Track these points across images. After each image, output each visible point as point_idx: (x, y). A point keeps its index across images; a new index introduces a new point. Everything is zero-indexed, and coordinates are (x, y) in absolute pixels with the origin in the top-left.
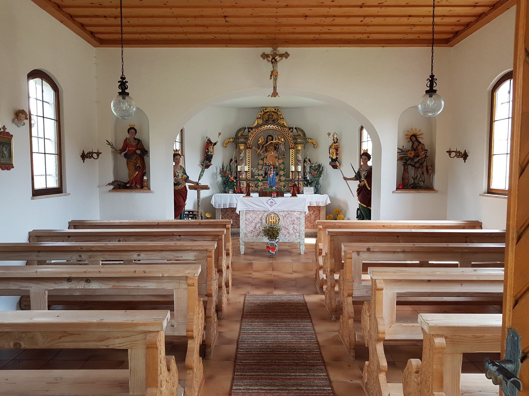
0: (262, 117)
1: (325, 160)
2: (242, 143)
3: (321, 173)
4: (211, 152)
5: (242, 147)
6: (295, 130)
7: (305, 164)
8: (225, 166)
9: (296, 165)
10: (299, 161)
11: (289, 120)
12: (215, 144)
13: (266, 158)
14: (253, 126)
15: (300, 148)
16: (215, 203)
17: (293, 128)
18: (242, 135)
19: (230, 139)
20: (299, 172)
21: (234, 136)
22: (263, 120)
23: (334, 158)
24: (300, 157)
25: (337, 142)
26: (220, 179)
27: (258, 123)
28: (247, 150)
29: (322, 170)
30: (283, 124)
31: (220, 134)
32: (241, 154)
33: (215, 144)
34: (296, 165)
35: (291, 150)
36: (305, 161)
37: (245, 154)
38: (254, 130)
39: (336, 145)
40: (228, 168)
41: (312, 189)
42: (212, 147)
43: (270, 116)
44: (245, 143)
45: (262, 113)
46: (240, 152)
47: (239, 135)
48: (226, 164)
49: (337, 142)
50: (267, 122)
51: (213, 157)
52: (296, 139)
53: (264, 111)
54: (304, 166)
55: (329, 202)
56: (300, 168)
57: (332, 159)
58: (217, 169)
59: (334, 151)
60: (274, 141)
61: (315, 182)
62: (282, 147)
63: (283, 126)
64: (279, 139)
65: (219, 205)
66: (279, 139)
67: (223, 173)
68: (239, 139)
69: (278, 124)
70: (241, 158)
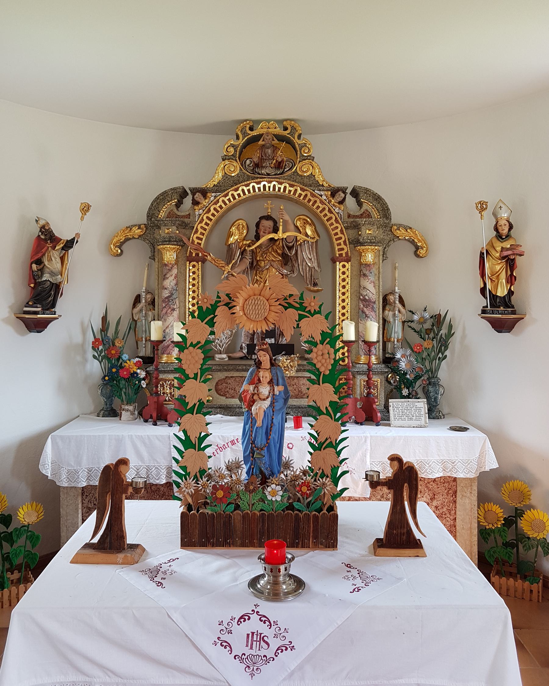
0: (241, 154)
1: (463, 305)
2: (371, 243)
3: (444, 344)
4: (52, 274)
5: (170, 255)
6: (350, 201)
7: (389, 314)
8: (112, 320)
9: (359, 317)
10: (367, 302)
11: (333, 164)
12: (69, 244)
13: (229, 306)
14: (211, 185)
15: (369, 257)
16: (56, 470)
17: (344, 191)
18: (170, 215)
19: (130, 228)
20: (369, 344)
21: (144, 220)
22: (243, 164)
23: (502, 292)
24: (372, 291)
25: (508, 236)
26: (95, 368)
27: (226, 176)
28: (189, 267)
29: (450, 334)
30: (312, 176)
31: (85, 209)
32: (165, 278)
33: (69, 244)
34: (359, 317)
35: (339, 266)
36: (385, 301)
37: (181, 279)
38: (211, 196)
39: (507, 245)
40: (124, 327)
41: (422, 405)
42: (55, 255)
43: (268, 148)
44: (181, 243)
45: (241, 142)
46: (163, 271)
47: (162, 215)
48: (121, 310)
49: (508, 236)
50: (255, 171)
51: (66, 288)
52: (356, 227)
53: (245, 134)
54: (384, 321)
55: (491, 463)
56: (373, 332)
57: (494, 297)
58: (84, 333)
59: (500, 266)
60: (280, 235)
61: (425, 377)
62: (307, 257)
63: (311, 183)
64: (297, 229)
65: (73, 474)
66: (297, 229)
67: (105, 343)
68: (165, 224)
69: (296, 178)
70: (166, 294)
